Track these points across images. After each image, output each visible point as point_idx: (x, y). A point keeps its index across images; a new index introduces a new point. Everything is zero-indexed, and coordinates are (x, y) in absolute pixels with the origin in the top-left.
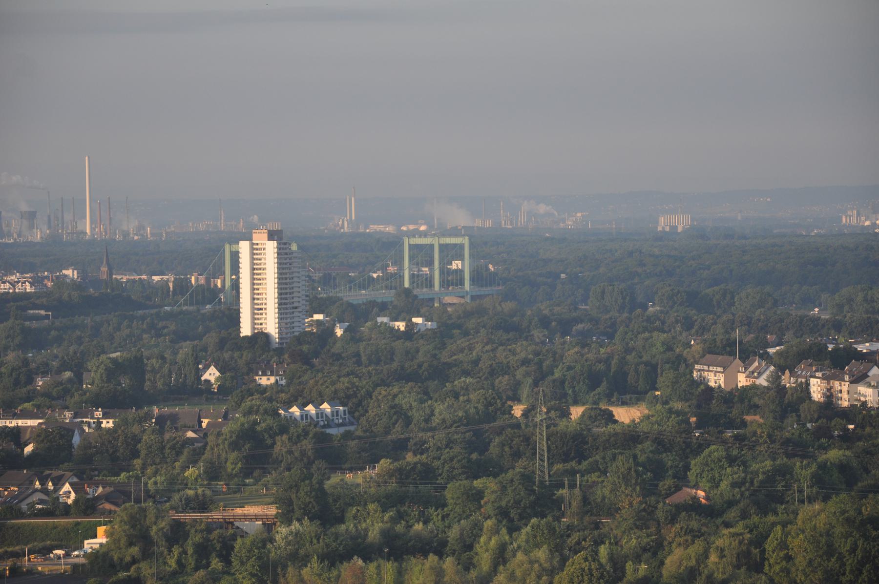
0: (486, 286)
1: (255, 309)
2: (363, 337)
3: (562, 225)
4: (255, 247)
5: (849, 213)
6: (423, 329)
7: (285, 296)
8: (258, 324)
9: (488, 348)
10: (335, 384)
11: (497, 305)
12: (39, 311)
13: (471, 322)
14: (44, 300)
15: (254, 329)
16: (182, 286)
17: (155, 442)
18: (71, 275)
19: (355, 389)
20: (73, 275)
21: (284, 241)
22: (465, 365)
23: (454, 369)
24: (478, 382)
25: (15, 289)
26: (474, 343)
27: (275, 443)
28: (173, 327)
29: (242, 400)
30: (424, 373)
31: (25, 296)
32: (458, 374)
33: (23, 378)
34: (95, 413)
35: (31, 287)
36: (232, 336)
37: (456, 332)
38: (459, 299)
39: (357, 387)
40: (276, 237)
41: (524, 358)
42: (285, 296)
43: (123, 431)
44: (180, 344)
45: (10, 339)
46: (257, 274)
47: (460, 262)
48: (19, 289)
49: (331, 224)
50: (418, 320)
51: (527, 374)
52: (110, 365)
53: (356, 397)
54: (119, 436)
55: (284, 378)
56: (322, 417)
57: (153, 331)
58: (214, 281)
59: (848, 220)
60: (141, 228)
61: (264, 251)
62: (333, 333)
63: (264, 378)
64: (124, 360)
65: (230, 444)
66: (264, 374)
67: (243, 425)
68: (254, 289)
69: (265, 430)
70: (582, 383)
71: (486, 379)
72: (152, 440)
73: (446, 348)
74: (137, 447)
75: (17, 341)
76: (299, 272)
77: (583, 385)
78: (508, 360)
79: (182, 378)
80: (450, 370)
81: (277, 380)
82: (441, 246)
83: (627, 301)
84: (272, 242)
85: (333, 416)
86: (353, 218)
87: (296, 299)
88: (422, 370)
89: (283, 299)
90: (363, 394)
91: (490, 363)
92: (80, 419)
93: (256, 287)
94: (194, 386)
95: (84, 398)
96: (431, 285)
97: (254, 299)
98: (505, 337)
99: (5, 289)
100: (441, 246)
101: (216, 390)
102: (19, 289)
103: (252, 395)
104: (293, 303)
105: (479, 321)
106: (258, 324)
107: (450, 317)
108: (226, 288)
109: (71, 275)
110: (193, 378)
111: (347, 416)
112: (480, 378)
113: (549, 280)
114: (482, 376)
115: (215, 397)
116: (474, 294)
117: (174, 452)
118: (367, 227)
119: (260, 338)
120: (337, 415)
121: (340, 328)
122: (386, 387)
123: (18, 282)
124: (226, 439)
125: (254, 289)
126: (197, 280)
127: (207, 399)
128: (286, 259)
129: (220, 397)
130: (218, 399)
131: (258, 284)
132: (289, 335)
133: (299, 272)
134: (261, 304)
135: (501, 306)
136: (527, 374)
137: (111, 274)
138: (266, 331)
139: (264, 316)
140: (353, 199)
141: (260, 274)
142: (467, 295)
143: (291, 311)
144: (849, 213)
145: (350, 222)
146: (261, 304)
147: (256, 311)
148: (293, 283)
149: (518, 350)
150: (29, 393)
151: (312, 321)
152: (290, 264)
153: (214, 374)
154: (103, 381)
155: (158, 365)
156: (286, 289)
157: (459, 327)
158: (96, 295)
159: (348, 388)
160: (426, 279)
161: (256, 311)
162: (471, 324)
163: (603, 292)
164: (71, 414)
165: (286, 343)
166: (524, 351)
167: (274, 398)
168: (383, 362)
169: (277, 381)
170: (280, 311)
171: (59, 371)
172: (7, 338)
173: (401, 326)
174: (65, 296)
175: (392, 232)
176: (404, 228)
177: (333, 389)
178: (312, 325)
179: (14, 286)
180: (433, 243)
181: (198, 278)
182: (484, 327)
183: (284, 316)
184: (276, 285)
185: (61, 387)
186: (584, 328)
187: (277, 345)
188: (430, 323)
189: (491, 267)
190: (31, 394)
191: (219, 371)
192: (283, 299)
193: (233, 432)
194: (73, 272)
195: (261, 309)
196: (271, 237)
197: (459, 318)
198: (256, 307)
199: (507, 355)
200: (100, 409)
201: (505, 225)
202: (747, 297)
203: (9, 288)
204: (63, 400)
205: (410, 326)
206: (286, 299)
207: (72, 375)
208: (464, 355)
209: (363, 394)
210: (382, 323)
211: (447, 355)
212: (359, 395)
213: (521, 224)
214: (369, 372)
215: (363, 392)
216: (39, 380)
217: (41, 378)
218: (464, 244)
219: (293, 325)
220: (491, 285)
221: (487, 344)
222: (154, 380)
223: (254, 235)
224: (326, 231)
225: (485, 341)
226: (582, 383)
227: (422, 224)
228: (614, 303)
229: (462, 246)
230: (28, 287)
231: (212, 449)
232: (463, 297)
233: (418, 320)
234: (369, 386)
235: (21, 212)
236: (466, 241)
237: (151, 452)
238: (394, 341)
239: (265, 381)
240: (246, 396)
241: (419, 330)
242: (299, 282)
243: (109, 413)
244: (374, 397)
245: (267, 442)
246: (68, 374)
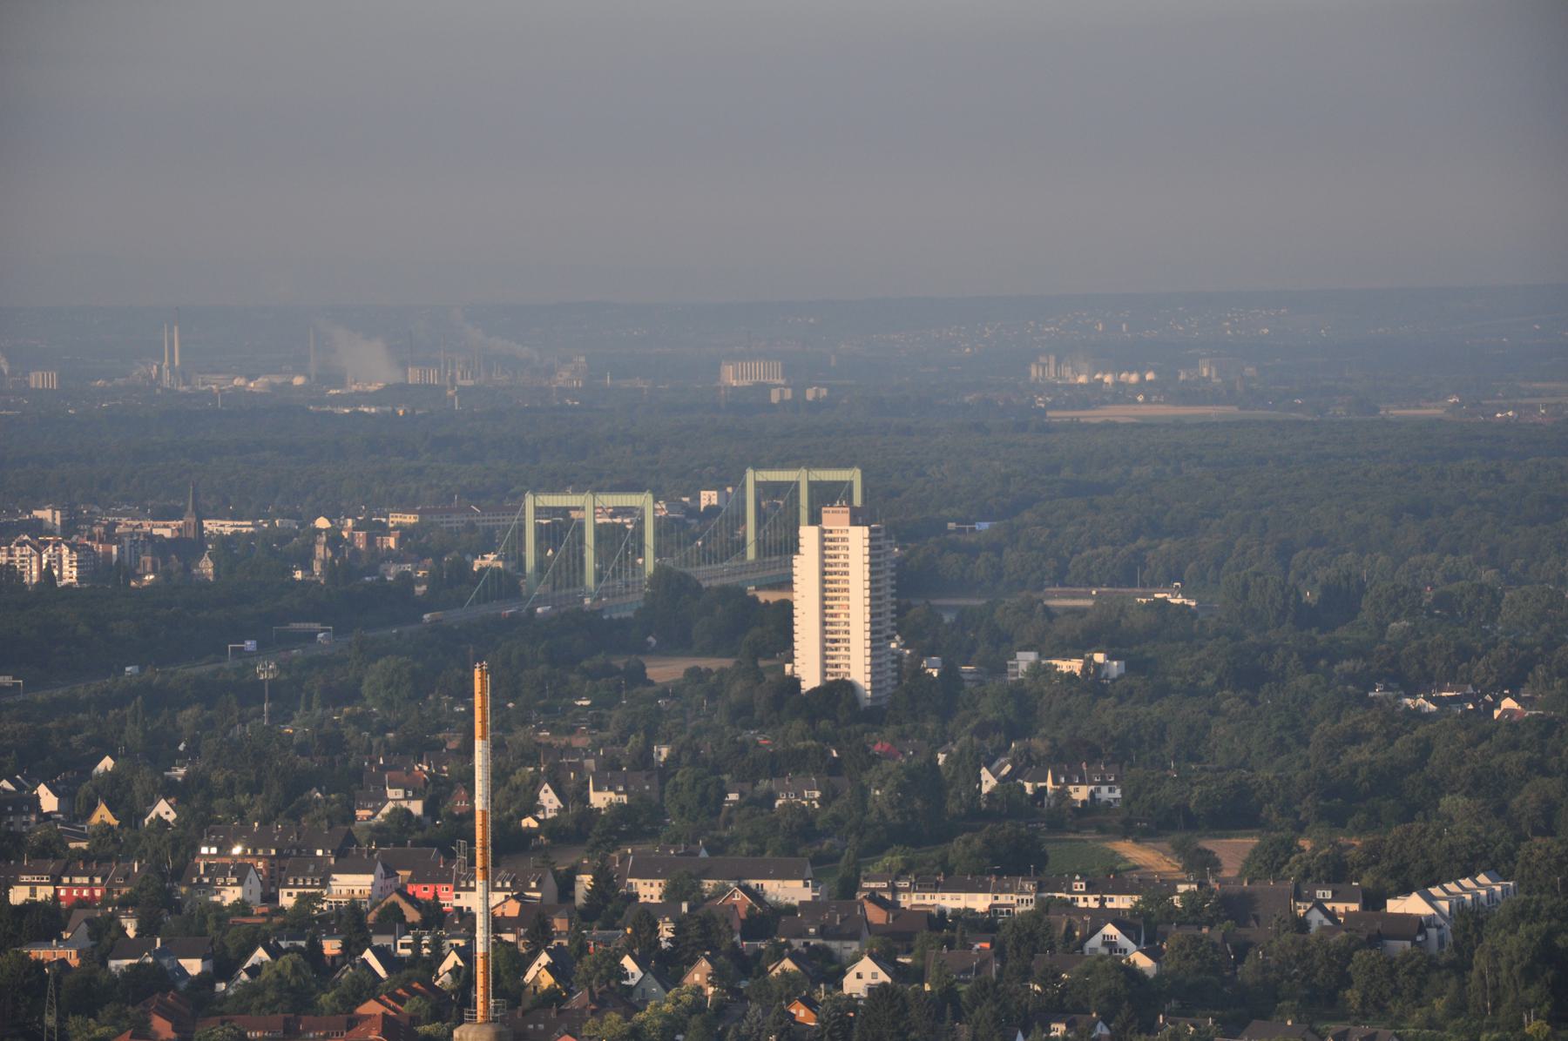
1: (826, 640)
4: (826, 535)
5: (1042, 359)
8: (832, 666)
18: (50, 520)
19: (1484, 845)
20: (54, 519)
30: (1363, 784)
32: (1419, 786)
39: (1485, 840)
46: (831, 582)
47: (715, 492)
56: (1493, 902)
58: (382, 540)
59: (1041, 373)
80: (1405, 779)
82: (813, 485)
84: (861, 528)
92: (1049, 894)
93: (827, 603)
100: (813, 485)
106: (832, 666)
109: (50, 520)
119: (837, 691)
131: (832, 599)
134: (836, 632)
138: (847, 678)
141: (836, 582)
144: (1042, 359)
146: (836, 632)
147: (828, 645)
159: (1472, 844)
161: (828, 645)
163: (1246, 587)
164: (1034, 885)
168: (1147, 744)
169: (1092, 794)
170: (873, 645)
172: (387, 687)
184: (867, 601)
187: (868, 703)
194: (54, 514)
195: (836, 641)
198: (828, 636)
201: (462, 378)
202: (1526, 599)
223: (825, 516)
236: (854, 476)
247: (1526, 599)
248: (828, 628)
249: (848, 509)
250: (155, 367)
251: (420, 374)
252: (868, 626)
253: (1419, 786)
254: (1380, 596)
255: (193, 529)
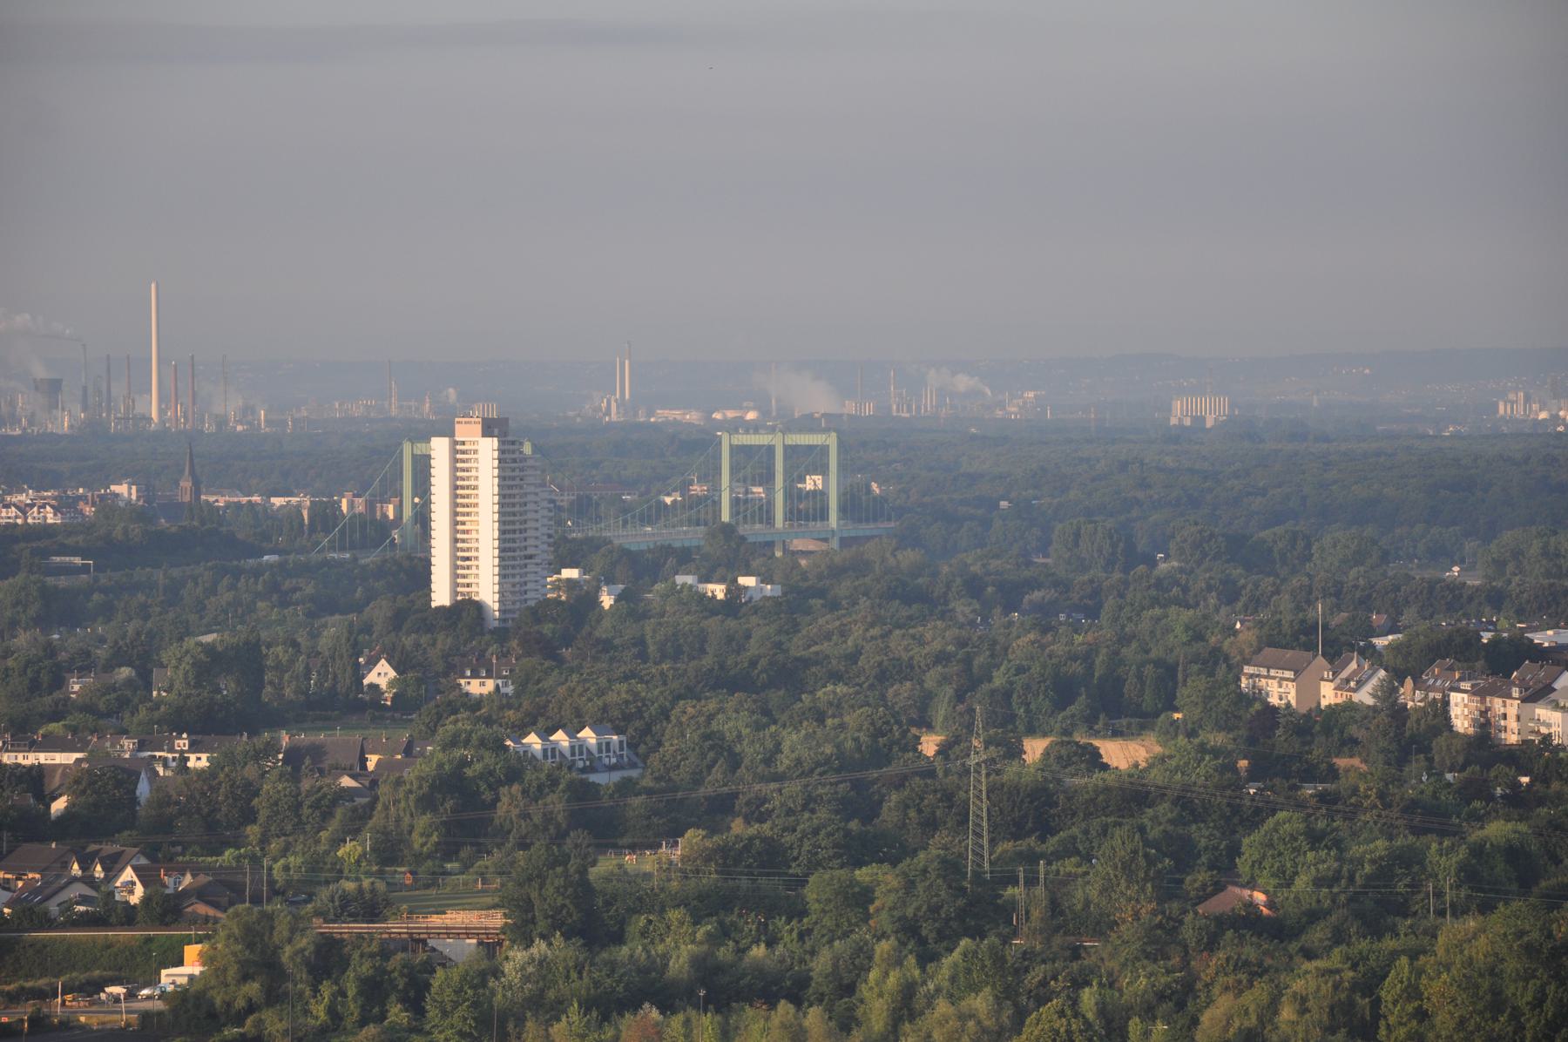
0: (867, 520)
1: (458, 558)
2: (649, 611)
3: (999, 413)
4: (458, 447)
5: (1512, 396)
6: (757, 597)
7: (511, 536)
8: (463, 585)
9: (875, 631)
10: (603, 694)
11: (888, 555)
12: (72, 558)
13: (844, 584)
14: (80, 538)
15: (457, 593)
16: (325, 517)
17: (285, 796)
18: (126, 495)
19: (640, 704)
20: (130, 494)
21: (510, 438)
22: (834, 662)
23: (814, 669)
24: (857, 693)
25: (26, 518)
26: (850, 623)
27: (498, 799)
28: (309, 590)
29: (438, 722)
31: (44, 531)
32: (821, 679)
33: (45, 678)
34: (177, 742)
35: (55, 515)
36: (416, 607)
37: (816, 603)
38: (819, 543)
39: (643, 700)
40: (496, 431)
41: (940, 651)
42: (511, 536)
43: (227, 775)
44: (323, 620)
45: (19, 608)
47: (820, 477)
48: (34, 518)
49: (587, 407)
50: (748, 581)
51: (945, 679)
52: (202, 656)
53: (642, 717)
54: (220, 783)
55: (510, 682)
56: (581, 753)
57: (275, 597)
58: (382, 507)
60: (248, 411)
61: (475, 456)
62: (596, 603)
63: (475, 682)
64: (227, 648)
65: (419, 800)
66: (475, 675)
67: (440, 766)
68: (457, 523)
69: (481, 776)
70: (1041, 697)
71: (872, 687)
72: (279, 792)
73: (799, 631)
74: (253, 803)
75: (32, 612)
76: (536, 494)
77: (1043, 699)
78: (911, 653)
79: (330, 681)
81: (497, 686)
82: (786, 448)
83: (1119, 551)
85: (600, 751)
86: (627, 397)
87: (531, 542)
88: (756, 671)
89: (509, 540)
90: (654, 713)
91: (878, 658)
92: (149, 753)
94: (351, 696)
95: (156, 715)
96: (769, 520)
97: (456, 540)
98: (905, 612)
99: (9, 518)
100: (786, 448)
101: (389, 703)
102: (34, 518)
103: (455, 712)
104: (526, 548)
105: (857, 583)
106: (463, 585)
107: (804, 575)
108: (404, 521)
109: (126, 495)
110: (348, 681)
111: (625, 753)
112: (860, 685)
113: (980, 512)
114: (864, 682)
115: (389, 714)
116: (845, 535)
117: (317, 813)
118: (651, 413)
119: (466, 610)
120: (608, 750)
121: (609, 594)
122: (695, 702)
123: (32, 506)
124: (410, 792)
125: (457, 523)
126: (351, 505)
127: (373, 719)
128: (513, 470)
129: (397, 715)
130: (393, 719)
131: (463, 514)
132: (518, 605)
133: (536, 494)
134: (468, 550)
135: (895, 556)
136: (945, 679)
137: (197, 492)
138: (476, 598)
139: (474, 571)
140: (627, 362)
141: (468, 496)
142: (833, 536)
143: (522, 562)
144: (1512, 396)
145: (621, 404)
146: (468, 550)
147: (459, 563)
148: (526, 512)
149: (928, 636)
150: (57, 704)
151: (559, 580)
152: (521, 480)
153: (386, 674)
154: (188, 684)
155: (286, 658)
156: (513, 523)
157: (821, 593)
158: (174, 529)
159: (627, 702)
160: (761, 508)
161: (459, 563)
162: (843, 588)
164: (134, 744)
165: (513, 619)
166: (939, 639)
167: (494, 717)
168: (686, 655)
169: (497, 687)
171: (109, 667)
173: (718, 590)
174: (118, 533)
175: (697, 423)
176: (717, 416)
177: (600, 703)
178: (559, 588)
179: (24, 513)
180: (773, 443)
181: (353, 502)
182: (866, 594)
183: (510, 571)
184: (496, 517)
185: (113, 696)
186: (1043, 598)
187: (496, 624)
188: (769, 587)
189: (874, 486)
190: (60, 707)
191: (395, 669)
192: (509, 540)
193: (423, 778)
194: (130, 489)
195: (468, 559)
196: (487, 432)
197: (820, 577)
198: (460, 554)
199: (909, 645)
200: (185, 735)
201: (898, 411)
203: (17, 517)
204: (117, 718)
205: (735, 591)
206: (514, 541)
207: (133, 674)
208: (832, 644)
209: (654, 713)
210: (684, 585)
211: (800, 643)
212: (646, 715)
213: (926, 410)
214: (662, 673)
215: (653, 709)
216: (74, 682)
217: (78, 678)
218: (774, 446)
219: (526, 588)
220: (875, 520)
221: (872, 625)
222: (279, 684)
223: (457, 426)
224: (578, 420)
225: (869, 620)
226: (1041, 697)
227: (748, 409)
228: (1096, 555)
229: (824, 450)
230: (50, 516)
231: (386, 808)
232: (825, 540)
233: (748, 581)
234: (665, 698)
235: (35, 380)
236: (831, 440)
237: (277, 813)
238: (706, 618)
239: (478, 687)
240: (445, 715)
241: (751, 598)
242: (536, 512)
243: (200, 742)
244: (672, 718)
245: (484, 797)
246: (125, 672)
247: (1335, 546)
248: (459, 545)
249: (480, 420)
250: (605, 400)
251: (856, 407)
252: (496, 543)
253: (821, 679)
254: (1185, 541)
255: (189, 492)
